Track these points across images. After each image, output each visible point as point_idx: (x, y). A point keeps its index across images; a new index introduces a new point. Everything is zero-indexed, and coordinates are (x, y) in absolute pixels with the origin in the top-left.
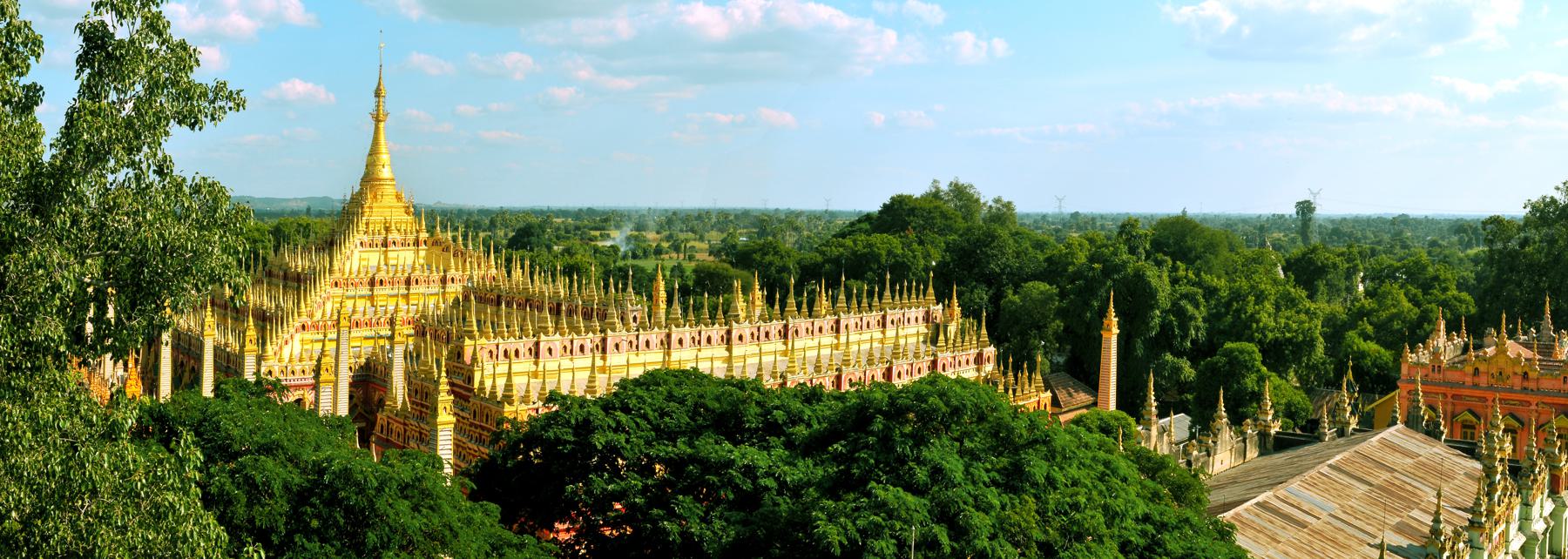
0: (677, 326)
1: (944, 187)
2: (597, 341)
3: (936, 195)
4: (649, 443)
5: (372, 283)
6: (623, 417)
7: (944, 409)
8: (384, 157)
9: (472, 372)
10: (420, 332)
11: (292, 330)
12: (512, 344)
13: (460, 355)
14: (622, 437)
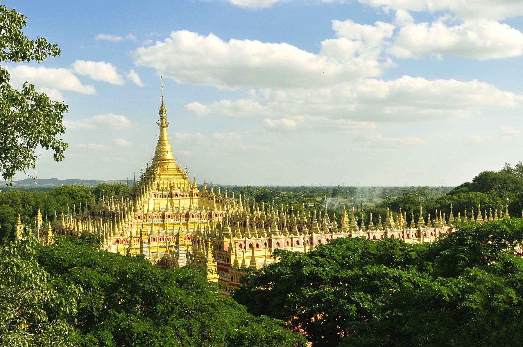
0: (355, 230)
1: (513, 167)
2: (307, 238)
3: (508, 171)
4: (336, 271)
5: (163, 217)
6: (321, 260)
7: (510, 232)
8: (167, 147)
9: (230, 256)
10: (196, 243)
11: (110, 243)
12: (254, 240)
13: (221, 247)
14: (321, 269)
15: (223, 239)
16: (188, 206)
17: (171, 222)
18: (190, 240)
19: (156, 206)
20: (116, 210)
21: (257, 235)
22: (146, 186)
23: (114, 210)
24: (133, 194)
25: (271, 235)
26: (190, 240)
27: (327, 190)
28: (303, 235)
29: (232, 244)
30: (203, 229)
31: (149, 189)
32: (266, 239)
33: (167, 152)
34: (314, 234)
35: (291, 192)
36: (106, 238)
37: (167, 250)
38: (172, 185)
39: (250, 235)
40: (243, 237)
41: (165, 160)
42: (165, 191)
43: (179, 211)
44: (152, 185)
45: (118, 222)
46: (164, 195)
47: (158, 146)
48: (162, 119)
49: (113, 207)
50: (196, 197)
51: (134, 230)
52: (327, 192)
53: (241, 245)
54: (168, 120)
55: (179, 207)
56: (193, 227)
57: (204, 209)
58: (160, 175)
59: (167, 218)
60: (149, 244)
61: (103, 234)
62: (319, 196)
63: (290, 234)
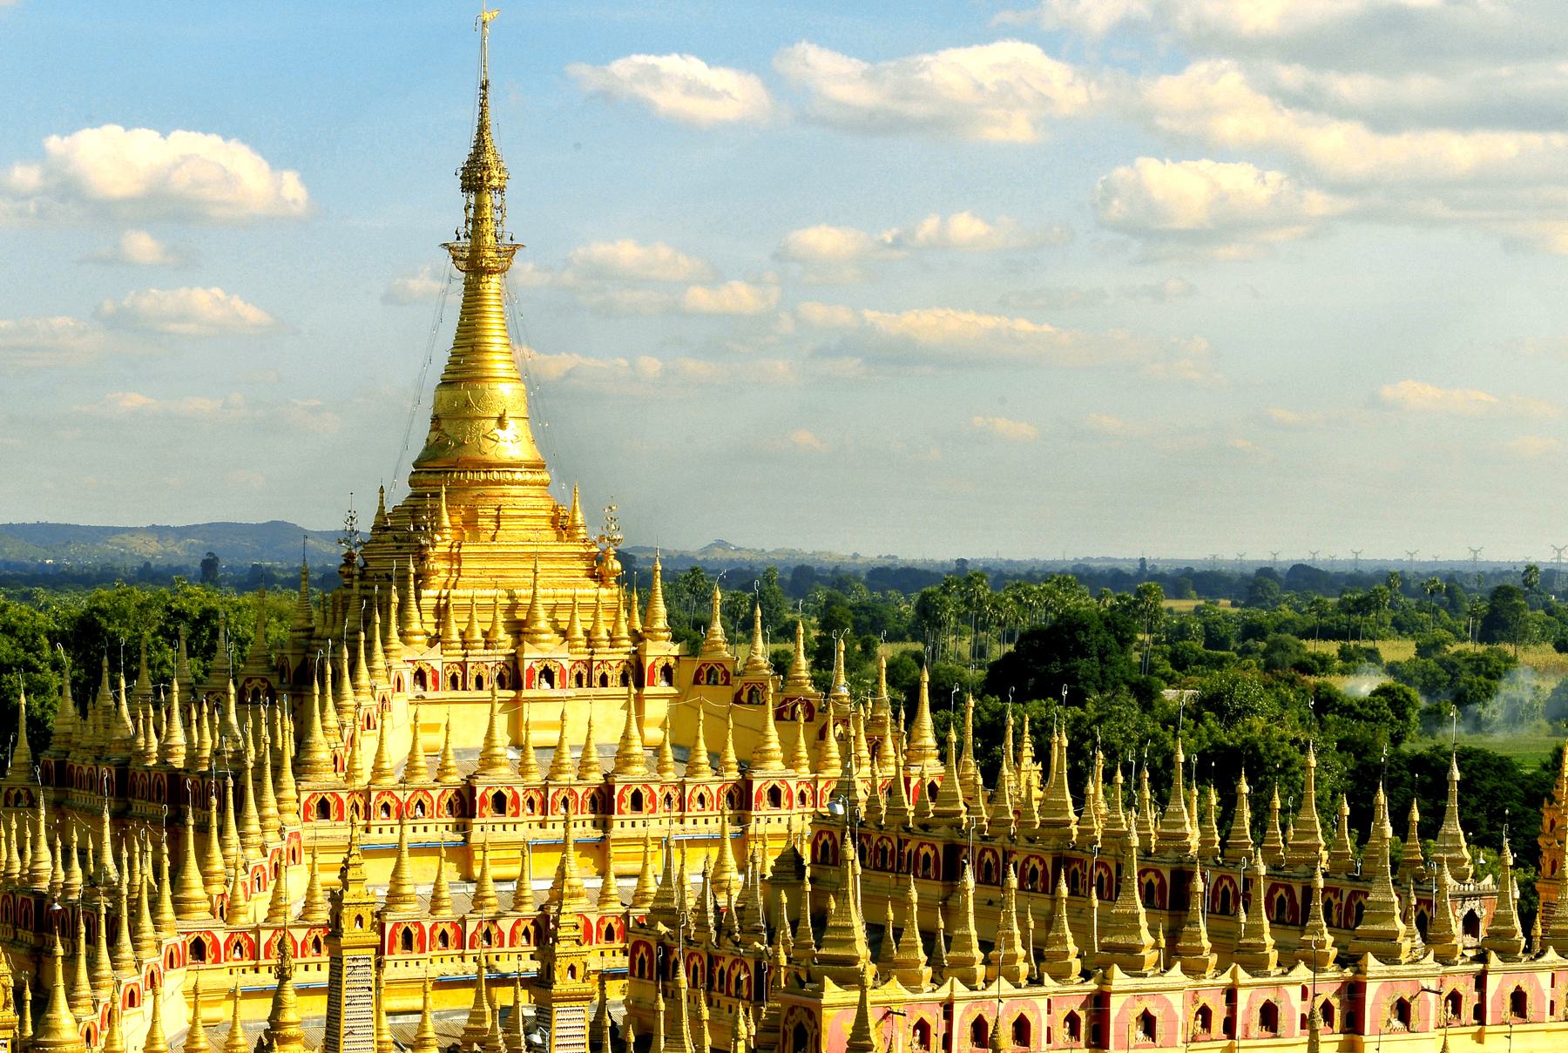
5: (464, 805)
8: (504, 390)
10: (651, 960)
15: (819, 993)
16: (615, 738)
17: (510, 835)
18: (618, 944)
19: (425, 739)
20: (193, 757)
21: (1024, 968)
22: (368, 622)
23: (179, 761)
24: (293, 663)
25: (1107, 966)
26: (618, 944)
27: (1449, 592)
28: (1302, 972)
29: (872, 1023)
30: (693, 880)
31: (385, 641)
32: (1076, 991)
33: (501, 421)
34: (1372, 964)
35: (1224, 605)
36: (135, 931)
37: (479, 993)
38: (521, 616)
39: (981, 970)
40: (937, 980)
41: (489, 466)
42: (478, 653)
43: (556, 768)
44: (403, 619)
45: (202, 830)
46: (472, 674)
47: (446, 383)
48: (477, 221)
49: (178, 740)
50: (662, 687)
51: (296, 882)
52: (1454, 607)
53: (923, 1027)
54: (514, 227)
55: (557, 748)
56: (636, 867)
57: (703, 758)
58: (454, 558)
59: (488, 810)
60: (379, 965)
61: (117, 905)
62: (1401, 627)
63: (1221, 968)
